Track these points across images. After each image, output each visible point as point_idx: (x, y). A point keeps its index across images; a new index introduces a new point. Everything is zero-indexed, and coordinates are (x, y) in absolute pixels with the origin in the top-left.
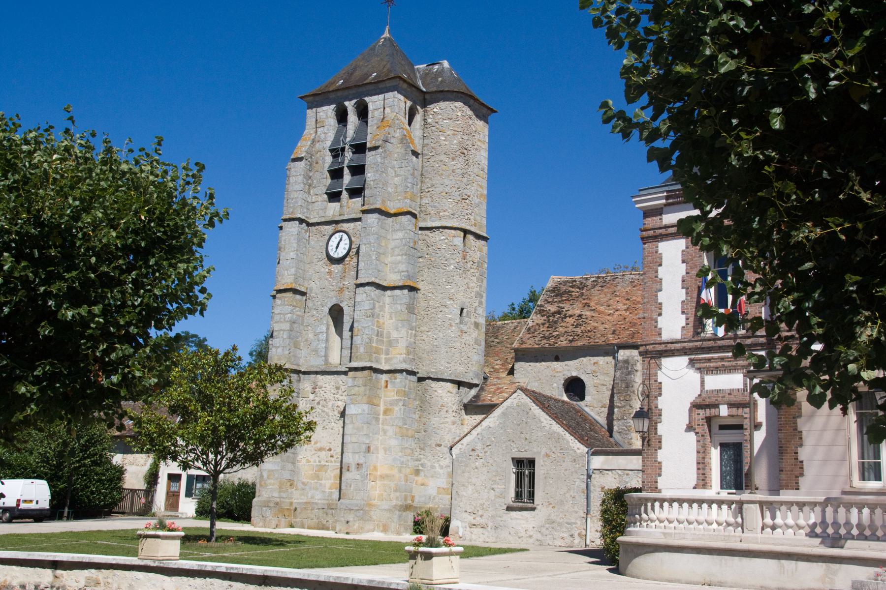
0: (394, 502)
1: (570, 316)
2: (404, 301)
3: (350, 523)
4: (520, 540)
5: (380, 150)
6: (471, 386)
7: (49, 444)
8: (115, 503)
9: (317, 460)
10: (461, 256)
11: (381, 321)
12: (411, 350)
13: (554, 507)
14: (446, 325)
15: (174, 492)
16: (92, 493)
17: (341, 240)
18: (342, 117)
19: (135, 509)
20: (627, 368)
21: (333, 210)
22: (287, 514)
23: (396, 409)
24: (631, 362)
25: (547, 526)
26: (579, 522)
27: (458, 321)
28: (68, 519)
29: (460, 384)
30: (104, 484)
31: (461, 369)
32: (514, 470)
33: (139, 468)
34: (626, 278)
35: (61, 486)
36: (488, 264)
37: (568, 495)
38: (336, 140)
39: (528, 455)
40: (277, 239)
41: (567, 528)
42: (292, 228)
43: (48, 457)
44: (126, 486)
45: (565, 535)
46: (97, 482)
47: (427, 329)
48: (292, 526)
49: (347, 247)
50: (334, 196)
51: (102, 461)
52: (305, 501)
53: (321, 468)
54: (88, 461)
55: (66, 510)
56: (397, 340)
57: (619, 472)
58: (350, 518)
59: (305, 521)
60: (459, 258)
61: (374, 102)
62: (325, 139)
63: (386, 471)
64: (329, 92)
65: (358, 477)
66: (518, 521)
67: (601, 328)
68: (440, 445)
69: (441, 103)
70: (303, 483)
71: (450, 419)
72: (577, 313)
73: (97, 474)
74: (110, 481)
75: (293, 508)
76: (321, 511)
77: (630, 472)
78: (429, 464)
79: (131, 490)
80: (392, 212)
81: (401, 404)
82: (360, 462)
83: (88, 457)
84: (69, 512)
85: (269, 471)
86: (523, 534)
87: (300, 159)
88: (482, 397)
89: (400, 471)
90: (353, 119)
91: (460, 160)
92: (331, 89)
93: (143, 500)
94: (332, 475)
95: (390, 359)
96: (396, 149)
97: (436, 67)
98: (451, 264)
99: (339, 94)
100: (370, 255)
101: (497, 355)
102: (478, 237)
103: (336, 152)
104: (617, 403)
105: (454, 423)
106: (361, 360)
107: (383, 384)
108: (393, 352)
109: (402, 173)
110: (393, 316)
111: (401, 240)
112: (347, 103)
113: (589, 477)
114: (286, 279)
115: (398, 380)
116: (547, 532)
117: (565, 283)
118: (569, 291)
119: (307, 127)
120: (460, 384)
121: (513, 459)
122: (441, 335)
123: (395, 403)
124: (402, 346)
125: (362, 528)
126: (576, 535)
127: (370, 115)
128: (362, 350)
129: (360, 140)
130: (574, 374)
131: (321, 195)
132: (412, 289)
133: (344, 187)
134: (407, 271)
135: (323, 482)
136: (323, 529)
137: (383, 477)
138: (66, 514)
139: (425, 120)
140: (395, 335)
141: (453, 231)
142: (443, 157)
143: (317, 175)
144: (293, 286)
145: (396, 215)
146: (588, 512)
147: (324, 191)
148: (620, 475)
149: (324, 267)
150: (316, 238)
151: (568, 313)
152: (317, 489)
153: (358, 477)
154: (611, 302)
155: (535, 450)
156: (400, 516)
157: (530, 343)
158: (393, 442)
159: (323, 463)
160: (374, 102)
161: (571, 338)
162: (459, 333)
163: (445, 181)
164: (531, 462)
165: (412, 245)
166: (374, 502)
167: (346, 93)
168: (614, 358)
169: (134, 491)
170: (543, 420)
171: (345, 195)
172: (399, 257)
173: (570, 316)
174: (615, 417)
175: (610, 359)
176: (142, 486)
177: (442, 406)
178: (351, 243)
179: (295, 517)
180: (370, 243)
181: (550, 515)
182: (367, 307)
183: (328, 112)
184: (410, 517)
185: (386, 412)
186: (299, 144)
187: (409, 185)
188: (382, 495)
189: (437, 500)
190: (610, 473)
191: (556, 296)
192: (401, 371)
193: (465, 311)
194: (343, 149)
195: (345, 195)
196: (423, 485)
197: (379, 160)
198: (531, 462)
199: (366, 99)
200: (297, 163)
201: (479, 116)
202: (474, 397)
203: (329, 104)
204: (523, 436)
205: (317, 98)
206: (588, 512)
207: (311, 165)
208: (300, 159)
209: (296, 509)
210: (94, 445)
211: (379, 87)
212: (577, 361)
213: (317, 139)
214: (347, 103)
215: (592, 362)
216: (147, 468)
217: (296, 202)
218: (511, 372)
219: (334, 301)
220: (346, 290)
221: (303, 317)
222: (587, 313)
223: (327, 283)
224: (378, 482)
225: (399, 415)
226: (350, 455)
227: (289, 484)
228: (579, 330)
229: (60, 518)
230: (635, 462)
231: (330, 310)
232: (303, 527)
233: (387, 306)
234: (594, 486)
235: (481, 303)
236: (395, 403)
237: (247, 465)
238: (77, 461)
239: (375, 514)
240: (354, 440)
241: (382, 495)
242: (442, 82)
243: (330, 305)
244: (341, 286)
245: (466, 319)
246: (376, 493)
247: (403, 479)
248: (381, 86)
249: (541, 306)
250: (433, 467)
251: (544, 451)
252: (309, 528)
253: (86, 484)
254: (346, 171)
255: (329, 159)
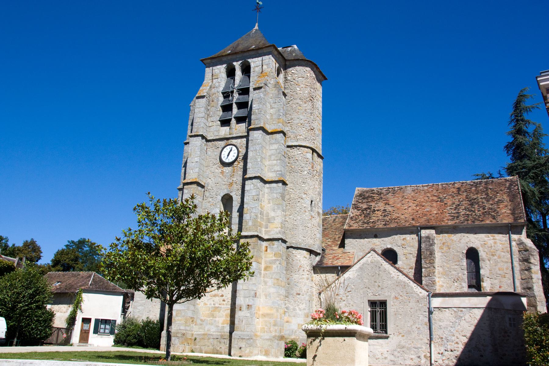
0: (273, 334)
1: (378, 210)
2: (279, 191)
3: (242, 349)
4: (377, 361)
5: (262, 89)
6: (317, 254)
7: (7, 292)
8: (47, 337)
9: (212, 303)
10: (311, 166)
11: (262, 204)
12: (283, 224)
13: (403, 336)
14: (302, 211)
15: (86, 330)
16: (32, 329)
17: (231, 150)
18: (231, 73)
19: (59, 342)
20: (429, 242)
21: (224, 131)
22: (189, 342)
23: (274, 266)
24: (432, 238)
25: (399, 350)
26: (424, 347)
27: (309, 209)
28: (16, 345)
29: (311, 252)
30: (41, 323)
31: (311, 242)
32: (370, 309)
33: (62, 314)
34: (409, 188)
35: (12, 324)
36: (323, 174)
37: (414, 327)
38: (227, 86)
39: (381, 298)
40: (182, 150)
41: (414, 351)
42: (197, 142)
43: (5, 302)
44: (55, 325)
45: (413, 357)
46: (36, 321)
47: (289, 214)
48: (193, 351)
49: (236, 155)
50: (225, 123)
51: (41, 307)
52: (203, 333)
53: (216, 309)
54: (34, 306)
55: (16, 340)
56: (274, 218)
57: (455, 309)
58: (243, 345)
59: (203, 348)
60: (310, 168)
61: (255, 63)
62: (219, 86)
63: (266, 311)
64: (223, 56)
65: (248, 315)
66: (375, 347)
67: (402, 217)
68: (299, 294)
69: (297, 67)
70: (201, 320)
71: (305, 276)
72: (382, 209)
73: (36, 316)
74: (45, 321)
75: (193, 338)
76: (216, 340)
77: (463, 309)
78: (292, 307)
79: (58, 328)
80: (270, 131)
81: (278, 262)
82: (250, 304)
83: (34, 303)
84: (17, 342)
85: (177, 310)
86: (380, 356)
87: (203, 97)
88: (325, 261)
89: (277, 311)
90: (238, 73)
91: (310, 103)
92: (224, 54)
93: (65, 335)
94: (224, 314)
95: (269, 231)
96: (271, 91)
97: (289, 49)
98: (305, 171)
99: (229, 57)
100: (256, 158)
101: (327, 236)
102: (319, 156)
103: (227, 95)
104: (424, 265)
105: (308, 279)
106: (250, 231)
107: (264, 248)
108: (271, 226)
109: (276, 106)
110: (271, 201)
111: (276, 150)
112: (235, 63)
113: (430, 313)
114: (191, 176)
115: (275, 246)
116: (399, 355)
117: (367, 192)
118: (372, 196)
119: (206, 79)
120: (311, 252)
121: (369, 301)
122: (299, 218)
123: (274, 262)
124: (277, 222)
125: (252, 353)
126: (422, 357)
127: (252, 70)
128: (250, 223)
129: (244, 86)
130: (389, 246)
131: (215, 122)
132: (284, 183)
133: (233, 116)
134: (281, 171)
135: (217, 319)
136: (217, 353)
137: (264, 315)
138: (15, 343)
139: (285, 78)
140: (272, 214)
141: (306, 149)
142: (298, 101)
143: (213, 109)
144: (197, 180)
145: (272, 133)
146: (431, 340)
147: (218, 119)
148: (455, 312)
149: (218, 169)
150: (212, 151)
151: (376, 209)
152: (212, 324)
153: (248, 315)
154: (403, 202)
155: (386, 294)
156: (278, 344)
157: (355, 226)
158: (272, 290)
159: (217, 305)
160: (255, 63)
161: (384, 223)
162: (310, 217)
163: (300, 116)
164: (383, 304)
165: (283, 154)
166: (258, 333)
167: (234, 57)
168: (417, 235)
169: (59, 329)
170: (391, 272)
171: (233, 121)
172: (275, 162)
173: (378, 210)
174: (423, 275)
175: (414, 236)
176: (64, 325)
177: (300, 266)
178: (238, 152)
179: (195, 344)
180: (256, 150)
181: (400, 342)
182: (254, 194)
183: (221, 70)
184: (282, 346)
185: (266, 269)
186: (201, 88)
187: (281, 114)
188: (264, 328)
189: (297, 333)
190: (447, 310)
191: (364, 199)
192: (277, 240)
193: (313, 202)
194: (232, 92)
195: (233, 121)
196: (287, 322)
197: (262, 96)
198: (383, 304)
199: (249, 60)
200: (200, 100)
201: (319, 81)
202: (319, 262)
203: (222, 64)
204: (376, 284)
205: (214, 61)
206: (431, 340)
207: (209, 102)
208: (203, 97)
209: (195, 339)
210: (38, 294)
211: (259, 52)
212: (391, 237)
213: (213, 86)
214: (235, 63)
215: (402, 238)
216: (67, 314)
217: (200, 125)
218: (342, 245)
219: (225, 192)
220: (234, 184)
221: (202, 202)
222: (388, 208)
223: (220, 180)
224: (260, 319)
225: (276, 270)
226: (242, 299)
227: (191, 321)
228: (387, 218)
229: (11, 345)
230: (467, 301)
231: (222, 198)
232: (201, 352)
233: (266, 194)
234: (435, 320)
235: (320, 199)
236: (274, 262)
237: (191, 298)
238: (26, 305)
239: (259, 342)
240: (245, 288)
241: (264, 328)
242: (295, 56)
243: (222, 195)
244: (231, 181)
245: (314, 209)
246: (259, 327)
247: (279, 316)
248: (260, 51)
249: (355, 205)
250: (294, 309)
251: (393, 295)
252: (206, 353)
253: (28, 323)
254: (234, 106)
255: (221, 99)
